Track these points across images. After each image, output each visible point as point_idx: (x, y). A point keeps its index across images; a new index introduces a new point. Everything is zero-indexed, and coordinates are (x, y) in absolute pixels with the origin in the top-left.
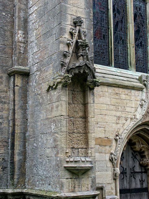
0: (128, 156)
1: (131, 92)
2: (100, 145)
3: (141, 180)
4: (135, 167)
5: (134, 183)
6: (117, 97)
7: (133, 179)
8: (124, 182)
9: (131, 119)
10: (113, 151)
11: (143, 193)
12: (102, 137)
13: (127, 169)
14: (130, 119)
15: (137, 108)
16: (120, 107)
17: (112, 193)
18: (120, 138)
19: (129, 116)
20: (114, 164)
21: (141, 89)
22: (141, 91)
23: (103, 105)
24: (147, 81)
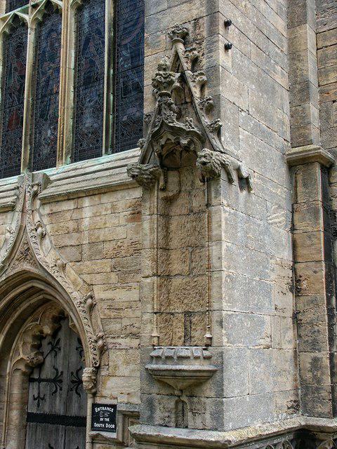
5: (77, 405)
7: (75, 396)
13: (65, 375)
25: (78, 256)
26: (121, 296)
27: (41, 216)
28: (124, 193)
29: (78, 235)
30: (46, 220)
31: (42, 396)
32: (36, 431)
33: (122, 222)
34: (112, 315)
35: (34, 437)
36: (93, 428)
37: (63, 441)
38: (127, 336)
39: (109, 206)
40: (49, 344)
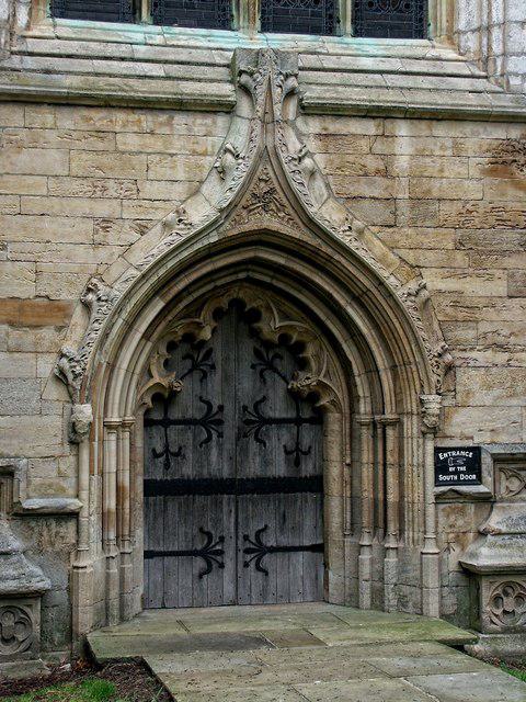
0: (238, 360)
1: (169, 123)
2: (11, 324)
3: (291, 446)
4: (269, 403)
5: (258, 459)
6: (100, 145)
7: (254, 446)
8: (208, 453)
9: (166, 225)
10: (69, 348)
11: (299, 494)
12: (23, 296)
13: (229, 408)
14: (159, 226)
15: (201, 182)
16: (111, 184)
17: (63, 490)
18: (99, 299)
19: (159, 215)
20: (71, 389)
21: (228, 109)
22: (227, 113)
23: (31, 180)
24: (251, 74)
25: (387, 217)
26: (474, 288)
27: (300, 135)
28: (479, 128)
29: (387, 182)
30: (312, 145)
31: (174, 449)
32: (165, 511)
33: (474, 172)
34: (460, 316)
35: (160, 520)
36: (438, 483)
37: (233, 520)
38: (487, 348)
39: (449, 143)
40: (184, 358)
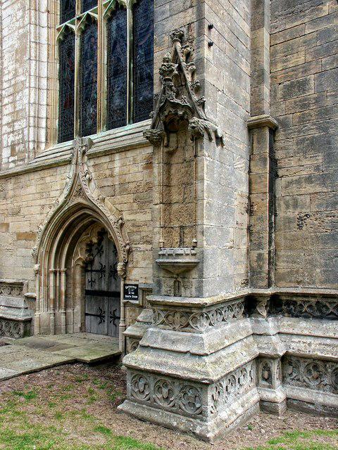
8: (101, 282)
13: (107, 266)
26: (141, 218)
28: (141, 150)
30: (91, 170)
33: (140, 169)
36: (125, 298)
